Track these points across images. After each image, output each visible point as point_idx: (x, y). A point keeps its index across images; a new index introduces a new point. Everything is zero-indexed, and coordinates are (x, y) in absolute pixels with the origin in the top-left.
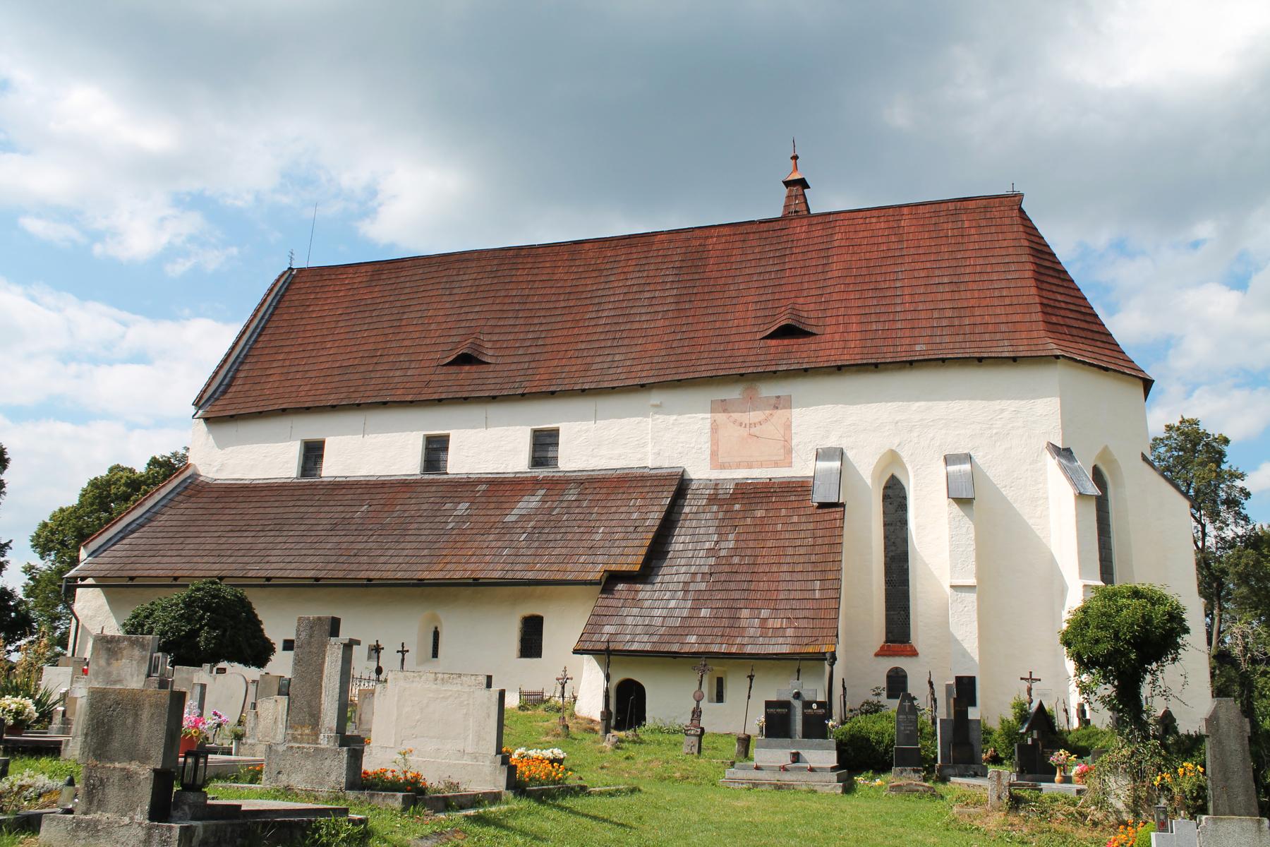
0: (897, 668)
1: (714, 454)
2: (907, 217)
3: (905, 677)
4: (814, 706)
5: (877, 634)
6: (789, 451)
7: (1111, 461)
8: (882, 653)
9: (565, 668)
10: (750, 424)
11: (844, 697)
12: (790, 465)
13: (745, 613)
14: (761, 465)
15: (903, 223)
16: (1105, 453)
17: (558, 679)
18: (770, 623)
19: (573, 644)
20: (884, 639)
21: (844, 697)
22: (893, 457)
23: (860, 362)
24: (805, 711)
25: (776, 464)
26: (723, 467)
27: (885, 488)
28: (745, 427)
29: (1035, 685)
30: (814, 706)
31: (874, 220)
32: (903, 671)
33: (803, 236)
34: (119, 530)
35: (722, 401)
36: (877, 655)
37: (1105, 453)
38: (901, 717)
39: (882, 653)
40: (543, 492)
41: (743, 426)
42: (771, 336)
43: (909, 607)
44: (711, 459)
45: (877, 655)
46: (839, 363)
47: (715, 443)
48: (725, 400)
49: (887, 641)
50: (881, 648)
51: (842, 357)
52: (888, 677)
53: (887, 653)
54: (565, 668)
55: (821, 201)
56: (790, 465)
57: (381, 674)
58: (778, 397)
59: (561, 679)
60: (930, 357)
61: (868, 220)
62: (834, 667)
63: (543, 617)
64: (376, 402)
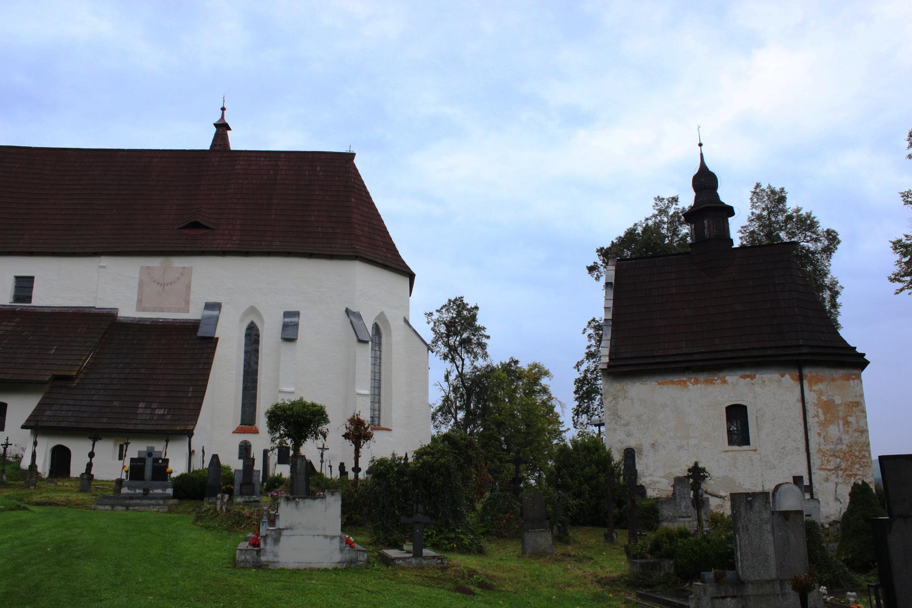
0: (245, 441)
1: (139, 301)
2: (283, 159)
3: (250, 446)
4: (160, 461)
5: (234, 417)
6: (187, 303)
7: (386, 321)
8: (238, 431)
9: (8, 437)
10: (164, 284)
11: (203, 458)
12: (188, 311)
13: (141, 405)
14: (169, 310)
15: (279, 163)
16: (382, 315)
17: (2, 445)
18: (157, 412)
19: (23, 422)
20: (239, 423)
21: (203, 458)
22: (253, 310)
23: (237, 250)
24: (143, 464)
25: (179, 310)
26: (144, 310)
27: (248, 329)
28: (161, 285)
29: (325, 452)
30: (160, 461)
31: (262, 159)
32: (249, 442)
33: (216, 164)
34: (382, 355)
35: (148, 267)
36: (234, 432)
37: (382, 315)
38: (211, 468)
39: (238, 431)
40: (18, 320)
41: (160, 284)
42: (207, 228)
43: (256, 404)
44: (137, 304)
45: (234, 432)
46: (224, 250)
47: (140, 294)
48: (149, 267)
49: (241, 425)
50: (237, 428)
51: (228, 246)
52: (240, 446)
53: (240, 431)
54: (8, 437)
55: (237, 142)
56: (188, 311)
57: (90, 452)
58: (184, 268)
59: (4, 445)
60: (324, 253)
61: (258, 159)
62: (192, 439)
63: (7, 404)
64: (106, 252)
